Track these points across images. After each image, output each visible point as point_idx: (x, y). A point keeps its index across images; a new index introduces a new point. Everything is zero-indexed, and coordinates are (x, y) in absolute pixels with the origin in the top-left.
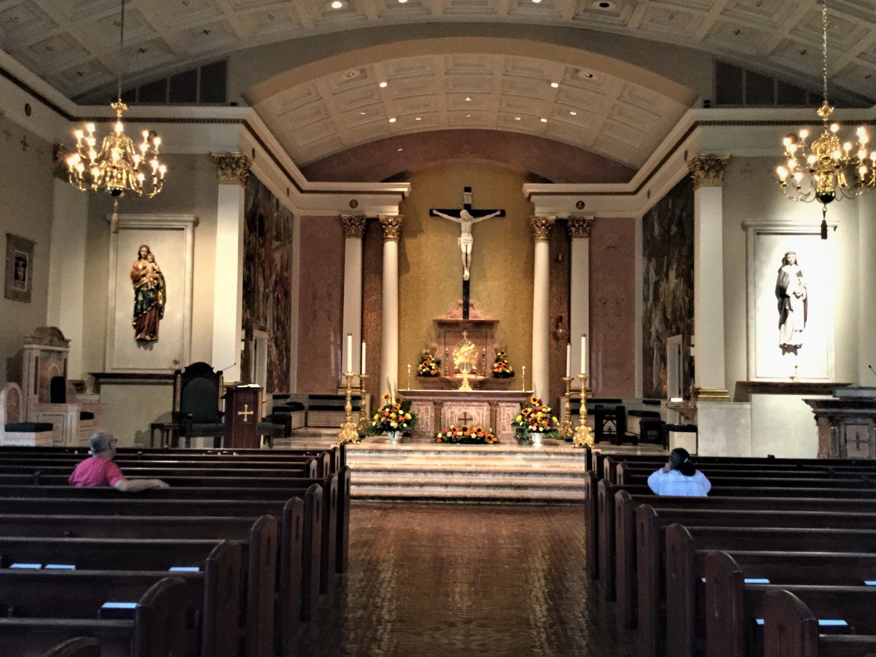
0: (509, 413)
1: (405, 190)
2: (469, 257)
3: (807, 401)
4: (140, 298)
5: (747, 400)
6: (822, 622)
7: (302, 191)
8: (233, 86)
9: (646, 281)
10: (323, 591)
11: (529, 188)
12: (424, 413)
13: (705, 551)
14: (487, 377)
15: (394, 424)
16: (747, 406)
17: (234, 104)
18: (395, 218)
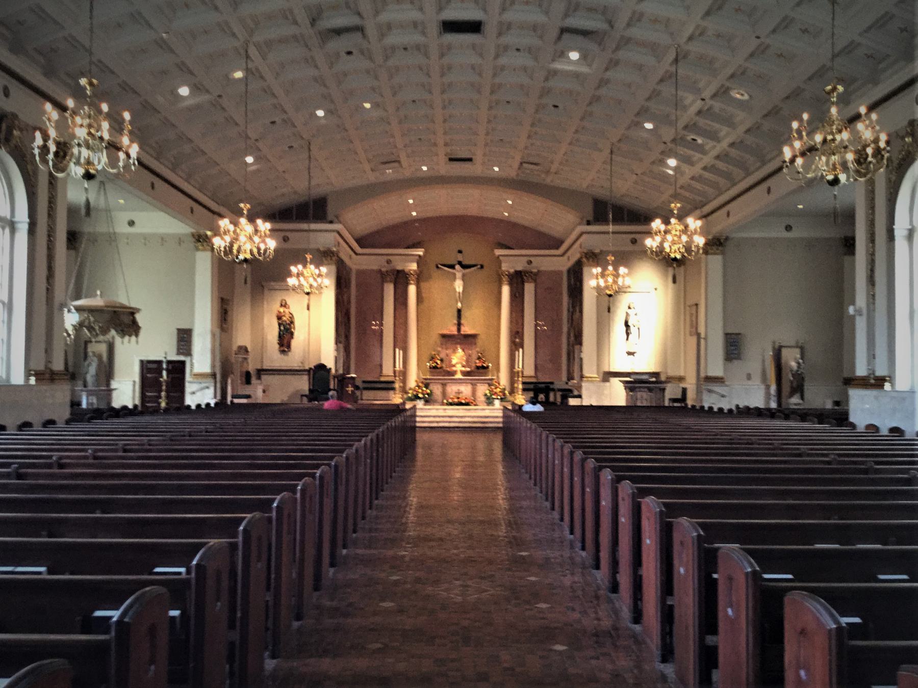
0: (482, 389)
1: (421, 253)
2: (461, 295)
3: (621, 381)
4: (282, 328)
5: (608, 381)
6: (766, 576)
7: (356, 254)
8: (331, 210)
9: (568, 310)
10: (371, 508)
11: (498, 252)
12: (437, 390)
13: (717, 545)
14: (473, 369)
15: (420, 395)
16: (607, 384)
17: (331, 222)
18: (415, 271)
